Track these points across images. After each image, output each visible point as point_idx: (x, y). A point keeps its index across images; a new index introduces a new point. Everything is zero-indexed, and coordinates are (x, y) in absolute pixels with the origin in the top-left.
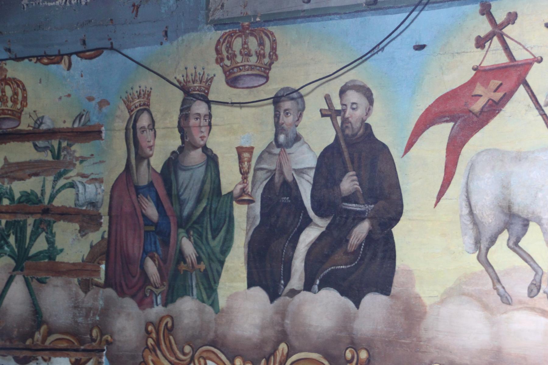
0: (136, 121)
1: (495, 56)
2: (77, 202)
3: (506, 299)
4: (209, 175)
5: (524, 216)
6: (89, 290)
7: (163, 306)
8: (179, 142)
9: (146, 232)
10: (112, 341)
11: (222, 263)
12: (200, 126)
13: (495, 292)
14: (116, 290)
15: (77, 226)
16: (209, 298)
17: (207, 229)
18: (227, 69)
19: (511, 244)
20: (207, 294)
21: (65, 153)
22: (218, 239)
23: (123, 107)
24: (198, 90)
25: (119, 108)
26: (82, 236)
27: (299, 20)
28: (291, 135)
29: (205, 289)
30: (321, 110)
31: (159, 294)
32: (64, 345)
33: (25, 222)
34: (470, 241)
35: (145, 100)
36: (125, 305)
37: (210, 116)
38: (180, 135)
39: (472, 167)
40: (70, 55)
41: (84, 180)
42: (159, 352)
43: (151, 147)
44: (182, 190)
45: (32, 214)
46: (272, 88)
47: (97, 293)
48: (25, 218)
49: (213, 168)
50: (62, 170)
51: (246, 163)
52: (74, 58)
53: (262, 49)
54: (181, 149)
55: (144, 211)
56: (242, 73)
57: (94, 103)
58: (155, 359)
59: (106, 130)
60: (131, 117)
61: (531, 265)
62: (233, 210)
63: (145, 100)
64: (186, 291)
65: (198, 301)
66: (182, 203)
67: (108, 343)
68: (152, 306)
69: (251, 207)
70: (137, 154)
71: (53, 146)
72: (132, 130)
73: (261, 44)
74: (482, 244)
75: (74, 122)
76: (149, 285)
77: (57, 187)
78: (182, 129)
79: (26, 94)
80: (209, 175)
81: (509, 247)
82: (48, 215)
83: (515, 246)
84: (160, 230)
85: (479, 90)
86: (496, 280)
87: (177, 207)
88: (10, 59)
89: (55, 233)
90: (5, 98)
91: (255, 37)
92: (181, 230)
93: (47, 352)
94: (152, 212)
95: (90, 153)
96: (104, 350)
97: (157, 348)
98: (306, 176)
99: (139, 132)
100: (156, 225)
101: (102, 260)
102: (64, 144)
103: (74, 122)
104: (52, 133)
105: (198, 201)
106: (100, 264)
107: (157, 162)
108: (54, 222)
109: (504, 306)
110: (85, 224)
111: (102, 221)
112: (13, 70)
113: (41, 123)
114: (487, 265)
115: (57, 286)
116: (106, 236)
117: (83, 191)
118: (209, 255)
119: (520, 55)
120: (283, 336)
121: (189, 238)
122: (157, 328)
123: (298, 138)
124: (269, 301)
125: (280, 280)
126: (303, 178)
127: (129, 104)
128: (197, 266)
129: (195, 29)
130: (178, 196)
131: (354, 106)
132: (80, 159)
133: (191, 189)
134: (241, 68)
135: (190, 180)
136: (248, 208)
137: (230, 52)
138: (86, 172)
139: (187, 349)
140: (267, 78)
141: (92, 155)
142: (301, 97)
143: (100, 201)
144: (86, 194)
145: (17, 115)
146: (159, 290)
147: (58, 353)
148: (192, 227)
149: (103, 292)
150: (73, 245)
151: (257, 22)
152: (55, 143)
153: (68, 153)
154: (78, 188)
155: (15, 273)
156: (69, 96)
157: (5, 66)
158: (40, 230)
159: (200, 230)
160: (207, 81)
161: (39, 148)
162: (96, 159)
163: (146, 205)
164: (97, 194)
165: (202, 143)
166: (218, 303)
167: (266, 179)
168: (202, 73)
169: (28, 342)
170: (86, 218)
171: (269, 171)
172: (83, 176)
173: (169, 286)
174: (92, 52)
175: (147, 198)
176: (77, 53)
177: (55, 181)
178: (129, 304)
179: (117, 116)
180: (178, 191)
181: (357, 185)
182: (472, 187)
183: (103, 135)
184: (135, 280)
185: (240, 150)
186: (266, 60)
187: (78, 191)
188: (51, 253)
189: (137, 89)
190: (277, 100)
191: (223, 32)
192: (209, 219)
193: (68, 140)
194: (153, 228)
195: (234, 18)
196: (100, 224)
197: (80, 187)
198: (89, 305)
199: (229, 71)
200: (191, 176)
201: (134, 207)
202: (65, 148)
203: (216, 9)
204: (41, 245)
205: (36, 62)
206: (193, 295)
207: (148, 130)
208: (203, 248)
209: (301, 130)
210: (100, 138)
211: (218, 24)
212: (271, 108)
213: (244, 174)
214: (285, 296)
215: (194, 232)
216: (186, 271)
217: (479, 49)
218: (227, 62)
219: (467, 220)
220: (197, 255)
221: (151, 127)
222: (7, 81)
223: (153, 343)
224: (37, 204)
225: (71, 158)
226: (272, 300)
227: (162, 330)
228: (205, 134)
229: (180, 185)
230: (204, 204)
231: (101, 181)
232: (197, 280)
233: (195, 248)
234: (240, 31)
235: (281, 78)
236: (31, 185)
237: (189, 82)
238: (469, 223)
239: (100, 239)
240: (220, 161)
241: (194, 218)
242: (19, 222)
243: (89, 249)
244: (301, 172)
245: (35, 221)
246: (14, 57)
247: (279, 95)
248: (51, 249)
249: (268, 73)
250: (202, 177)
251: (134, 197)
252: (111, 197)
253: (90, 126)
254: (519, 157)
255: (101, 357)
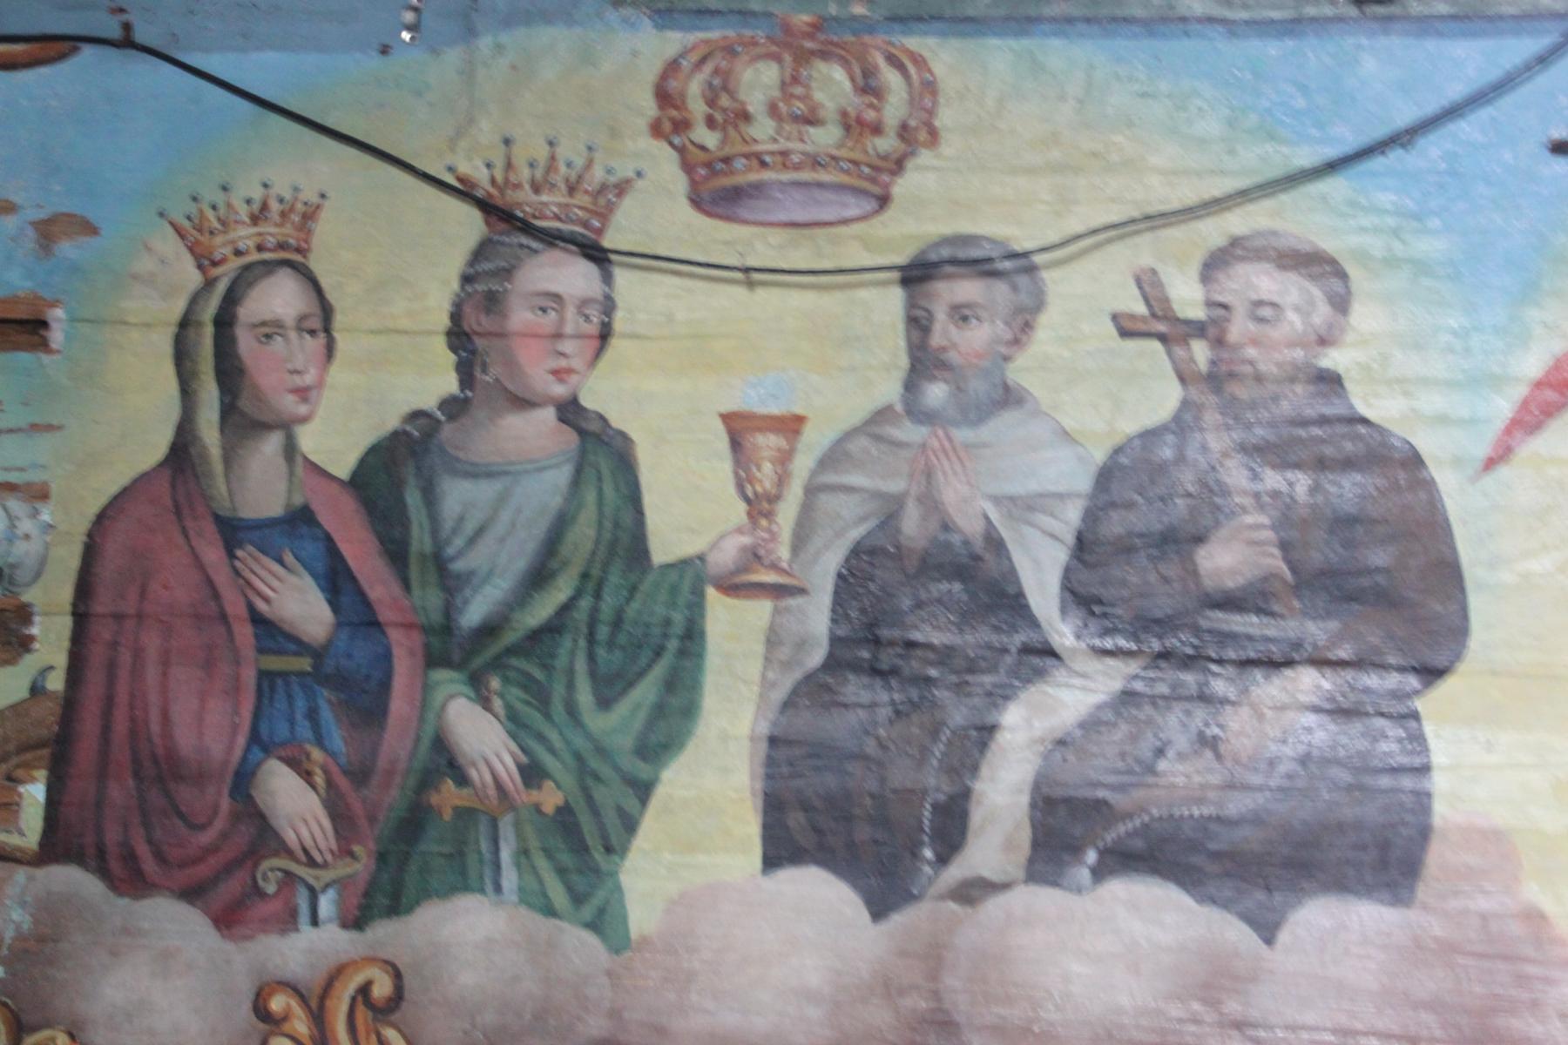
4: (590, 497)
7: (345, 925)
8: (449, 383)
12: (558, 336)
14: (104, 873)
16: (578, 899)
17: (570, 672)
20: (570, 889)
22: (623, 708)
23: (169, 245)
24: (557, 218)
25: (148, 249)
27: (1046, 27)
28: (978, 387)
30: (1115, 318)
31: (327, 886)
35: (288, 229)
36: (146, 925)
37: (609, 306)
46: (907, 228)
49: (606, 472)
51: (767, 467)
53: (871, 106)
54: (454, 407)
55: (261, 606)
59: (73, 319)
60: (209, 284)
62: (702, 616)
63: (288, 229)
64: (463, 874)
65: (523, 910)
66: (452, 584)
69: (788, 610)
70: (228, 411)
72: (209, 330)
73: (869, 87)
76: (276, 854)
78: (458, 336)
80: (590, 497)
84: (338, 668)
87: (430, 599)
91: (845, 63)
94: (303, 605)
101: (28, 766)
105: (539, 577)
111: (35, 630)
116: (56, 683)
118: (579, 757)
122: (314, 1004)
123: (1009, 397)
124: (865, 915)
127: (204, 239)
128: (523, 796)
130: (439, 562)
131: (1266, 312)
133: (502, 540)
134: (768, 159)
135: (502, 505)
136: (777, 611)
137: (724, 101)
140: (884, 201)
142: (1031, 269)
148: (497, 664)
149: (31, 879)
151: (854, 18)
159: (538, 674)
163: (275, 583)
165: (559, 390)
166: (624, 919)
168: (579, 162)
171: (877, 495)
173: (382, 857)
175: (281, 562)
178: (174, 922)
179: (135, 277)
181: (1272, 555)
183: (56, 336)
184: (206, 838)
185: (738, 428)
186: (886, 144)
189: (248, 188)
190: (917, 275)
192: (582, 643)
194: (305, 664)
196: (25, 644)
199: (708, 165)
200: (502, 499)
201: (210, 582)
206: (498, 888)
207: (293, 335)
208: (553, 736)
209: (1022, 371)
210: (44, 346)
213: (759, 507)
214: (942, 897)
216: (466, 815)
218: (711, 139)
220: (524, 759)
226: (879, 909)
227: (344, 1008)
228: (577, 363)
229: (448, 525)
230: (560, 592)
231: (39, 494)
237: (518, 186)
244: (1025, 507)
247: (933, 257)
250: (556, 502)
251: (213, 554)
252: (91, 552)
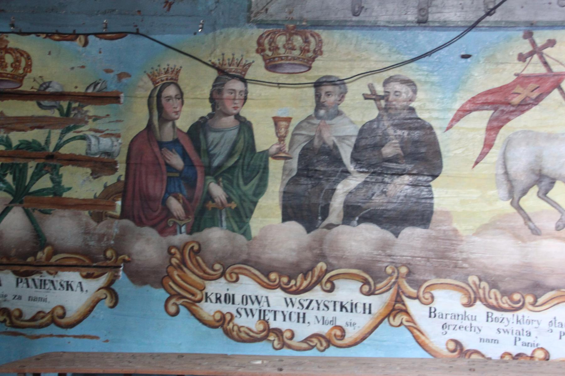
0: (161, 91)
1: (535, 67)
2: (89, 151)
3: (536, 232)
4: (242, 136)
5: (552, 176)
6: (102, 221)
8: (210, 110)
9: (169, 177)
10: (130, 259)
11: (255, 204)
12: (234, 99)
13: (527, 227)
14: (134, 220)
15: (89, 171)
16: (240, 228)
17: (238, 177)
18: (268, 58)
19: (540, 195)
20: (238, 226)
21: (76, 112)
22: (250, 185)
23: (146, 79)
24: (234, 72)
26: (95, 178)
28: (332, 111)
29: (236, 222)
30: (363, 94)
32: (74, 262)
33: (25, 166)
34: (503, 192)
37: (246, 92)
38: (210, 104)
39: (508, 143)
40: (86, 35)
41: (98, 135)
42: (185, 269)
43: (177, 113)
44: (212, 147)
45: (34, 159)
46: (316, 74)
47: (112, 223)
48: (25, 162)
50: (72, 125)
51: (283, 129)
52: (91, 38)
56: (283, 62)
57: (112, 74)
58: (181, 273)
60: (156, 88)
61: (557, 209)
63: (173, 75)
64: (214, 223)
66: (211, 157)
67: (124, 261)
68: (175, 233)
69: (287, 162)
70: (160, 117)
71: (61, 106)
74: (515, 194)
75: (88, 88)
77: (65, 139)
78: (212, 99)
79: (31, 62)
80: (242, 136)
81: (539, 197)
82: (52, 161)
83: (544, 195)
85: (518, 89)
86: (527, 219)
87: (206, 160)
88: (13, 32)
89: (62, 175)
90: (4, 64)
92: (208, 177)
93: (53, 268)
94: (177, 161)
95: (107, 114)
96: (121, 267)
97: (182, 266)
98: (347, 142)
99: (164, 101)
100: (181, 172)
101: (118, 197)
102: (75, 105)
103: (88, 88)
104: (61, 95)
105: (230, 155)
106: (114, 200)
107: (184, 123)
108: (61, 166)
109: (534, 236)
110: (97, 169)
111: (118, 167)
112: (13, 41)
113: (48, 87)
114: (519, 209)
115: (64, 216)
116: (123, 179)
117: (97, 143)
119: (556, 68)
120: (322, 257)
121: (218, 183)
122: (181, 251)
123: (339, 113)
125: (318, 216)
126: (345, 143)
129: (236, 25)
131: (398, 94)
132: (93, 118)
135: (222, 139)
136: (285, 163)
138: (101, 128)
139: (217, 266)
141: (108, 115)
143: (117, 151)
144: (100, 145)
145: (20, 79)
146: (183, 222)
147: (66, 268)
149: (119, 222)
150: (81, 184)
152: (64, 104)
153: (79, 112)
154: (90, 140)
155: (12, 205)
156: (83, 67)
157: (5, 38)
158: (43, 172)
159: (230, 177)
160: (245, 65)
161: (44, 106)
162: (113, 119)
164: (112, 146)
165: (235, 112)
167: (305, 141)
168: (240, 59)
169: (30, 260)
170: (101, 164)
172: (96, 131)
173: (195, 219)
174: (114, 35)
175: (171, 151)
176: (96, 34)
177: (63, 134)
179: (139, 86)
180: (208, 147)
182: (509, 155)
183: (122, 100)
184: (157, 213)
185: (277, 120)
186: (310, 54)
187: (91, 143)
188: (57, 190)
189: (164, 66)
190: (318, 85)
191: (266, 30)
193: (80, 102)
194: (177, 175)
195: (278, 21)
196: (116, 170)
197: (93, 141)
198: (102, 232)
200: (222, 137)
202: (75, 109)
203: (258, 13)
204: (45, 182)
205: (45, 38)
206: (222, 226)
209: (342, 107)
210: (119, 102)
211: (260, 24)
212: (311, 91)
213: (281, 139)
215: (223, 179)
216: (214, 209)
217: (521, 62)
219: (502, 178)
221: (179, 96)
222: (8, 50)
223: (177, 262)
224: (40, 151)
225: (83, 116)
226: (309, 231)
228: (239, 105)
230: (235, 159)
231: (118, 136)
232: (227, 214)
233: (225, 191)
234: (284, 30)
235: (321, 68)
236: (31, 135)
237: (225, 65)
238: (503, 180)
239: (116, 181)
240: (255, 127)
241: (224, 169)
242: (18, 164)
243: (102, 189)
244: (342, 138)
245: (38, 165)
246: (18, 31)
248: (57, 187)
249: (311, 64)
253: (107, 92)
254: (550, 137)
255: (117, 272)
